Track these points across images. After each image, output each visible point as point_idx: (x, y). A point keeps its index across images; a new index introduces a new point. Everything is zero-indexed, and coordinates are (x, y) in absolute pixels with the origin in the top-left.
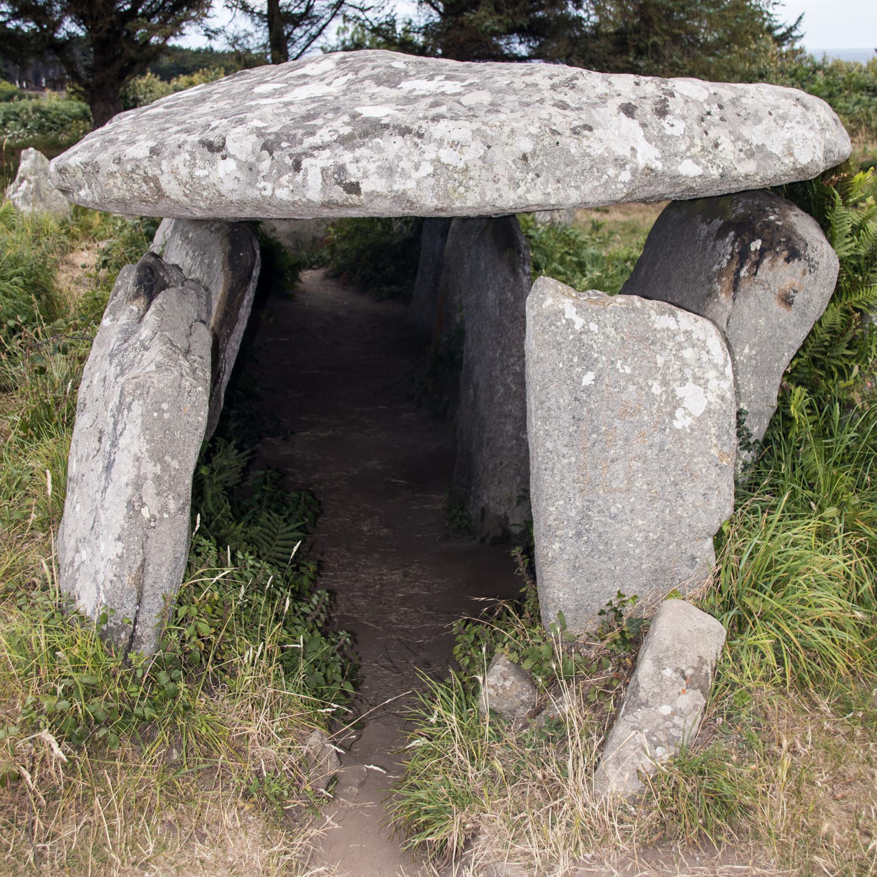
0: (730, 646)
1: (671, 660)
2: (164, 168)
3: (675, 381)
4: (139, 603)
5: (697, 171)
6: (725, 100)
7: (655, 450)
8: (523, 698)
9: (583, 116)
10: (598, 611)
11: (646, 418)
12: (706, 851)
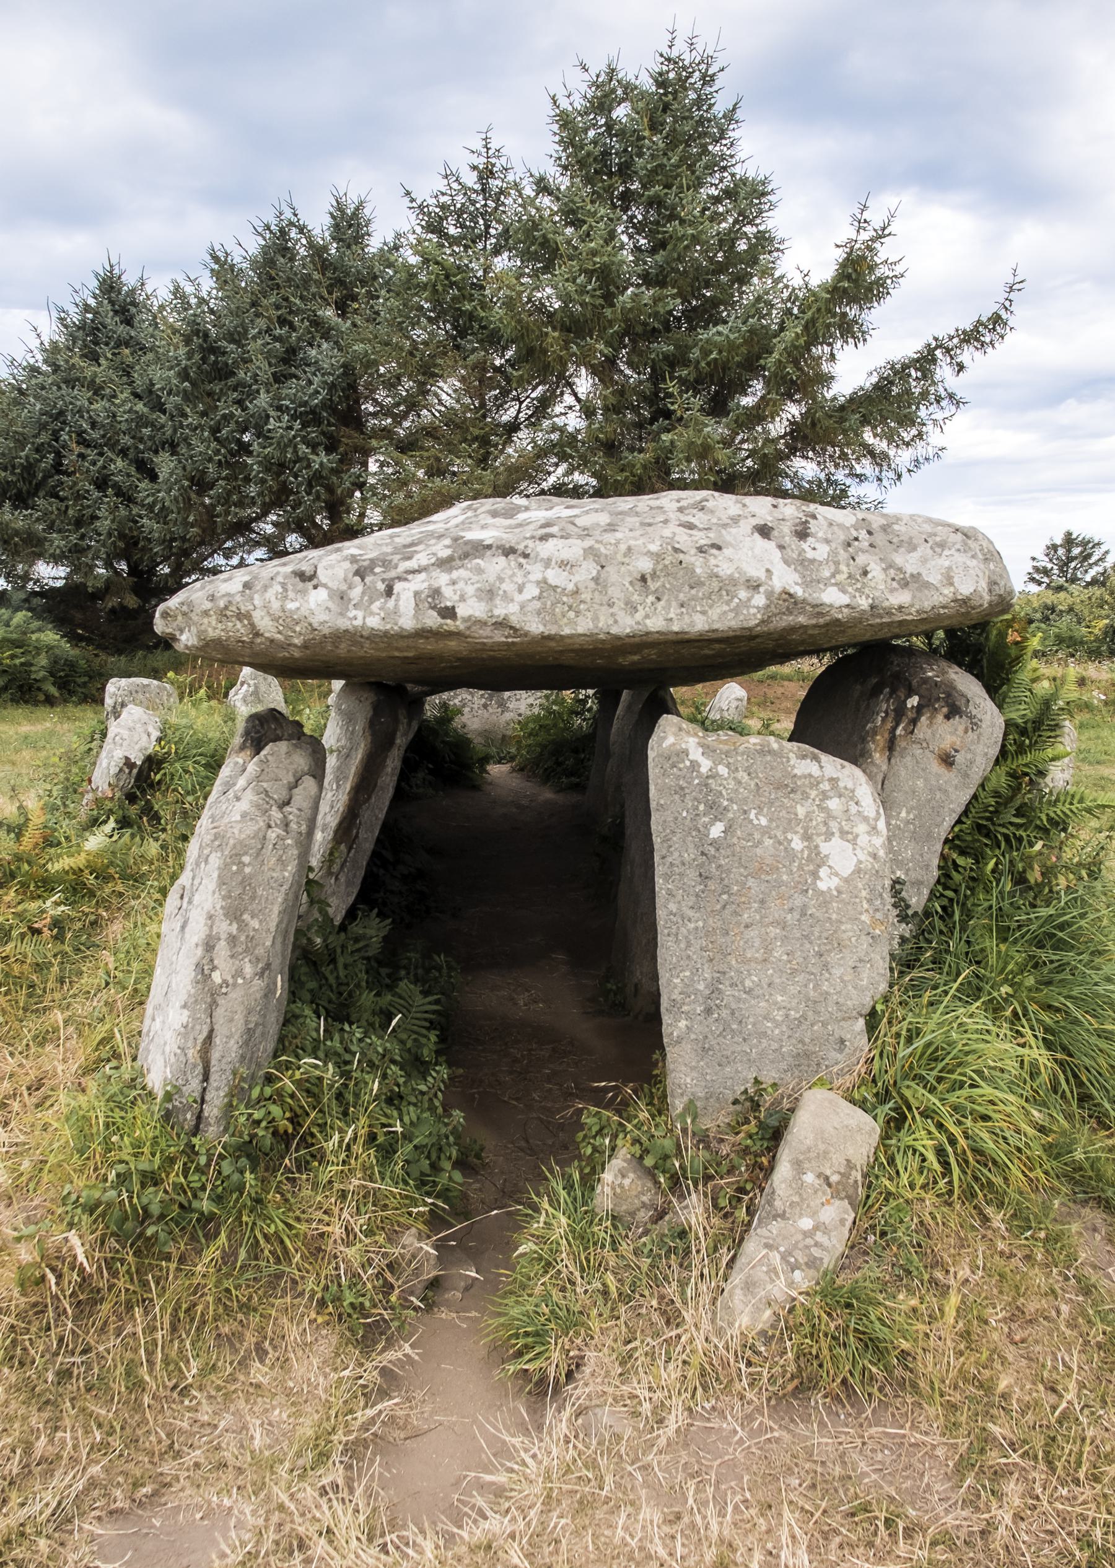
0: (884, 1145)
1: (814, 1164)
2: (256, 602)
3: (818, 835)
4: (206, 1078)
5: (845, 600)
6: (875, 526)
7: (796, 915)
8: (645, 1199)
9: (711, 535)
10: (731, 1100)
11: (785, 877)
12: (852, 1406)
